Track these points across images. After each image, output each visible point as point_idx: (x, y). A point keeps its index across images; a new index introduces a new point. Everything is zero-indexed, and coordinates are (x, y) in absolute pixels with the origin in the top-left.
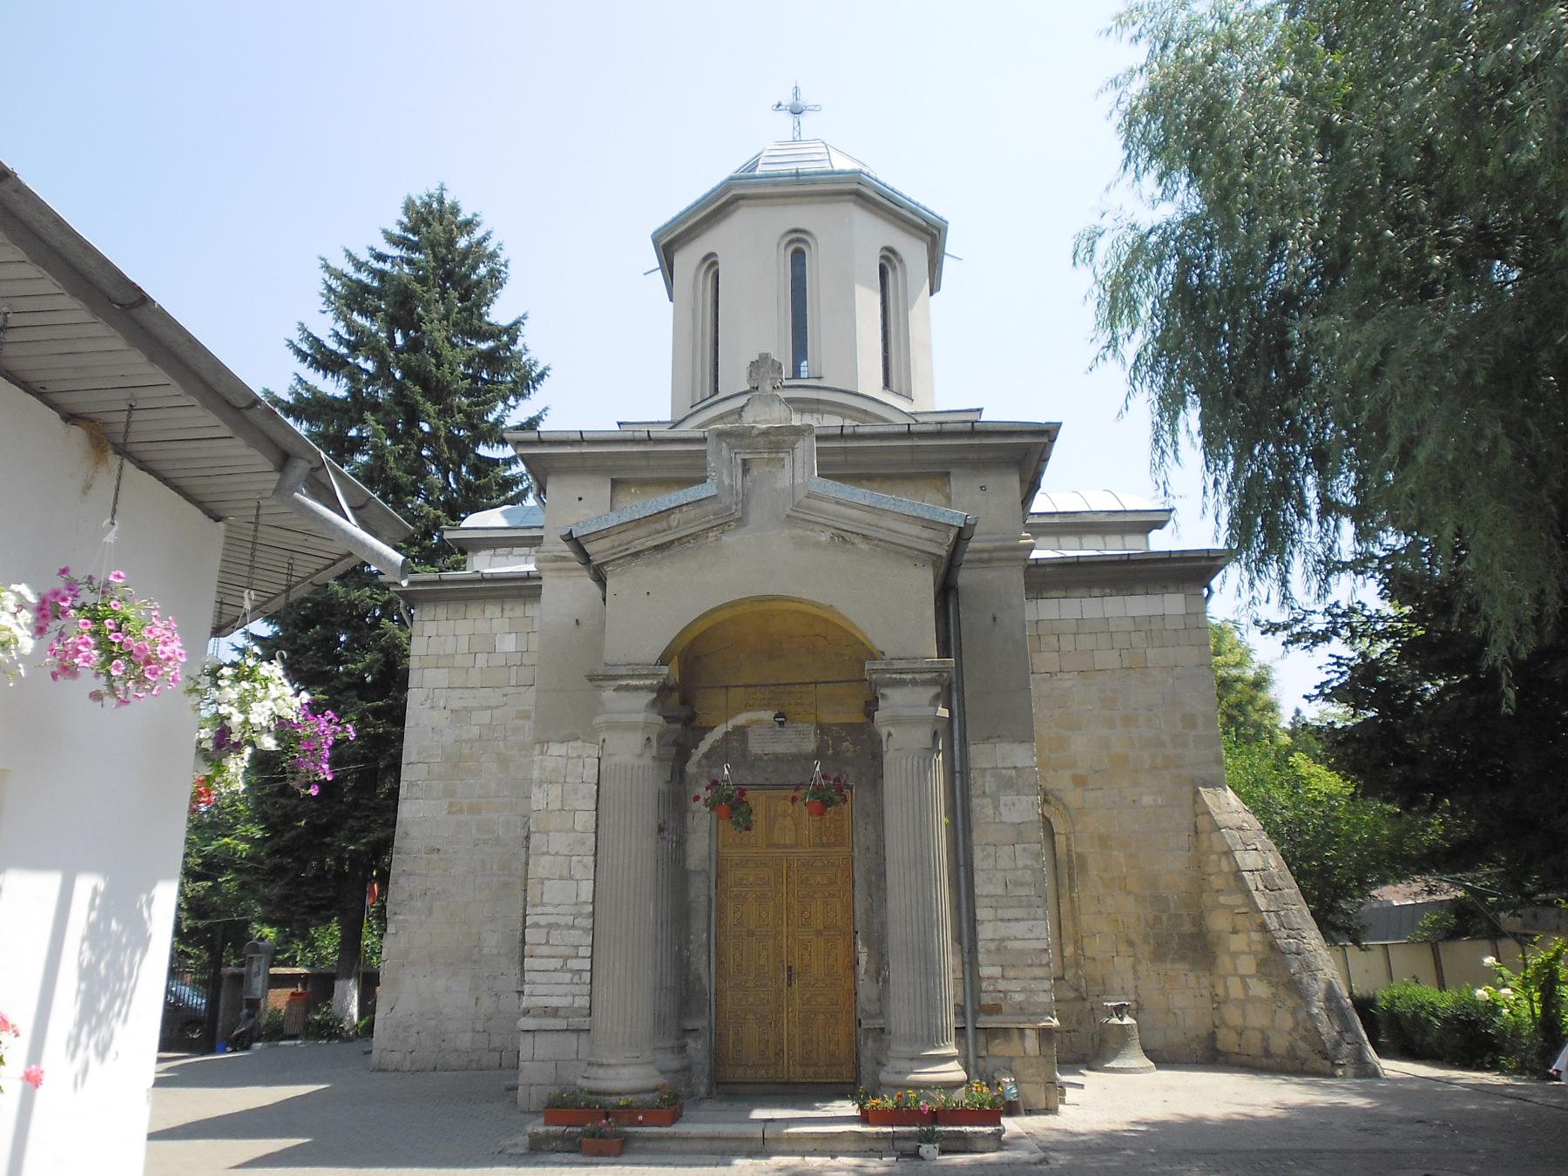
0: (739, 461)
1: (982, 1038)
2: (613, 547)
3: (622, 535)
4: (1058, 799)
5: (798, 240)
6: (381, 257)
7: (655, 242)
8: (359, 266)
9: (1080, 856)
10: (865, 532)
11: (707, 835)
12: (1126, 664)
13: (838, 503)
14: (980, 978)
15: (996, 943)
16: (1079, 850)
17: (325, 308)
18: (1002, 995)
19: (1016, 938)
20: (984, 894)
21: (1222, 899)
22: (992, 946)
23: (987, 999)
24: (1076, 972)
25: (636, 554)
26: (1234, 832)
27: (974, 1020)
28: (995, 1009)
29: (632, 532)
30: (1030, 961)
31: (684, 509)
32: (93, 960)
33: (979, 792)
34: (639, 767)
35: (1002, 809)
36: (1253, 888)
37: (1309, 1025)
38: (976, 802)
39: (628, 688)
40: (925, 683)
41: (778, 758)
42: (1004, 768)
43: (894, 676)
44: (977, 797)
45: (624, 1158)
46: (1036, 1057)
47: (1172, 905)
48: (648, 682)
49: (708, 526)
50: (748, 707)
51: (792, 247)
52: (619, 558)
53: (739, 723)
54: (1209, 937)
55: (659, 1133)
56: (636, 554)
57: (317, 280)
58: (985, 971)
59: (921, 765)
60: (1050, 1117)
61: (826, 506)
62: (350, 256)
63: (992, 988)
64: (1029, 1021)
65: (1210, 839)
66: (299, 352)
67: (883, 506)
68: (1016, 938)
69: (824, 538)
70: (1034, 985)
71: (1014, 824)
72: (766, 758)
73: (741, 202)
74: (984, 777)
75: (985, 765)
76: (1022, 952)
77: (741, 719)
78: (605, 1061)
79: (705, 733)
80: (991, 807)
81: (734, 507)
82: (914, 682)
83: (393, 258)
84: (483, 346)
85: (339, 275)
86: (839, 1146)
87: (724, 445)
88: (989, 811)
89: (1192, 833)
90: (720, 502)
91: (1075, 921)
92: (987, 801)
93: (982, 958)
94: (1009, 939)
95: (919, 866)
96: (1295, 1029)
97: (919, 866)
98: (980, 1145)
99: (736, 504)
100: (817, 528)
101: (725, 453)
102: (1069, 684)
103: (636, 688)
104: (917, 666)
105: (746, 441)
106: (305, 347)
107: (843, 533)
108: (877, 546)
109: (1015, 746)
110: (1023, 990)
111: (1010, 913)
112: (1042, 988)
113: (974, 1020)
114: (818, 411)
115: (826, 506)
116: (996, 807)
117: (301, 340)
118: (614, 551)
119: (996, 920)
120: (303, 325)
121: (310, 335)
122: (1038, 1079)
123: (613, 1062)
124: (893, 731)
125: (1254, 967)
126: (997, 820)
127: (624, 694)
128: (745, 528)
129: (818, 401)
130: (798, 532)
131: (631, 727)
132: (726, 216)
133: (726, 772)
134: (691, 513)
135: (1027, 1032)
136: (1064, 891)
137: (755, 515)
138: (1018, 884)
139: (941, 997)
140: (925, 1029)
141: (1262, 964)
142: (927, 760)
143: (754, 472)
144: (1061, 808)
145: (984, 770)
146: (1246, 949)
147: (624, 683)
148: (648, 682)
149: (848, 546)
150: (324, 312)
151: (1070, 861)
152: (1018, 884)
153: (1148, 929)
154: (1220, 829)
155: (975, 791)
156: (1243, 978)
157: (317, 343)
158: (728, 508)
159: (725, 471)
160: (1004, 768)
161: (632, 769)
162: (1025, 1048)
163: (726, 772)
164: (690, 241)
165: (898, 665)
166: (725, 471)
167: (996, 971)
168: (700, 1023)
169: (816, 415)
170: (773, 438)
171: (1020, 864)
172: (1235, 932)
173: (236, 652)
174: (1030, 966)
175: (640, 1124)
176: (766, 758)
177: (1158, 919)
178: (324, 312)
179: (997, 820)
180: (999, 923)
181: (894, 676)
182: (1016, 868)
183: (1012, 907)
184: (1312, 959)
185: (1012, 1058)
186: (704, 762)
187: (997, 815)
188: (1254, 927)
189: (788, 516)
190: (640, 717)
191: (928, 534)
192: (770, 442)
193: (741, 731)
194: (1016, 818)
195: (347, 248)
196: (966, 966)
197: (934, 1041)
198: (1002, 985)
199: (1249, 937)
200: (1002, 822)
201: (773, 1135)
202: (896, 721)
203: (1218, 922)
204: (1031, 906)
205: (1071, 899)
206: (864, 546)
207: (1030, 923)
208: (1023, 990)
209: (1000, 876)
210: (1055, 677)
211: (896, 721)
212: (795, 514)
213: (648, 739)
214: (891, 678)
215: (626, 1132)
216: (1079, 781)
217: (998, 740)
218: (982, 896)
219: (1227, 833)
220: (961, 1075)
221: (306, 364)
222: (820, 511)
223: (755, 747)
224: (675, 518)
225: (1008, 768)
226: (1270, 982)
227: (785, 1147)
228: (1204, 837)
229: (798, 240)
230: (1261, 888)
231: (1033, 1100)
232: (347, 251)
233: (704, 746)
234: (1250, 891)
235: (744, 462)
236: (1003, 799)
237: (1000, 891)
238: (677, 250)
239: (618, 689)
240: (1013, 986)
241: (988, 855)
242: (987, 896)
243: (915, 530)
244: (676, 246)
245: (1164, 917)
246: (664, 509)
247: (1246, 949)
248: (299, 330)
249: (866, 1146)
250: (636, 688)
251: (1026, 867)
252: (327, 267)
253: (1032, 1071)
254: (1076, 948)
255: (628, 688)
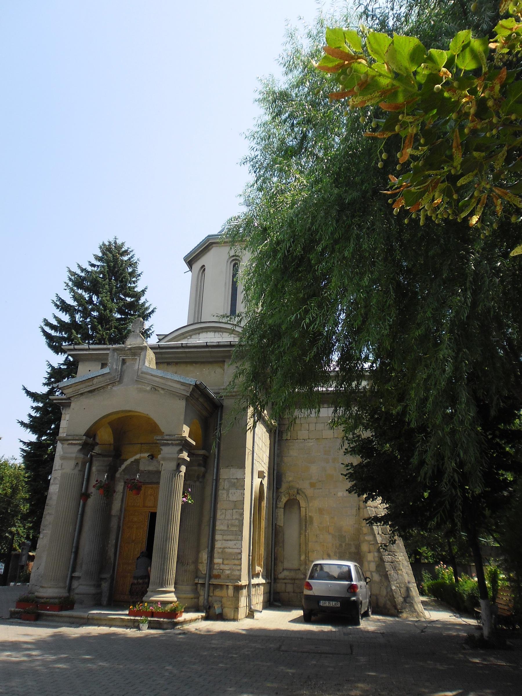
0: (121, 359)
1: (212, 588)
2: (73, 392)
3: (76, 387)
4: (303, 492)
5: (236, 259)
6: (93, 265)
7: (185, 259)
8: (83, 270)
9: (311, 517)
10: (163, 387)
11: (120, 501)
12: (335, 436)
13: (152, 375)
14: (214, 564)
15: (221, 549)
16: (310, 514)
17: (66, 288)
18: (221, 571)
19: (229, 548)
20: (219, 529)
21: (366, 538)
22: (220, 550)
23: (215, 572)
24: (305, 567)
25: (82, 394)
26: (373, 509)
27: (209, 581)
28: (218, 577)
29: (80, 386)
30: (233, 557)
31: (98, 377)
32: (149, 568)
33: (222, 488)
34: (74, 474)
35: (230, 495)
36: (376, 533)
37: (391, 594)
38: (220, 492)
39: (72, 444)
40: (177, 445)
41: (149, 472)
42: (232, 479)
43: (165, 442)
44: (221, 490)
45: (38, 622)
46: (232, 597)
47: (347, 540)
48: (79, 442)
49: (107, 384)
50: (141, 452)
51: (234, 262)
52: (76, 395)
53: (137, 458)
54: (361, 554)
55: (52, 614)
56: (82, 394)
57: (65, 277)
58: (216, 561)
59: (171, 476)
60: (235, 623)
61: (148, 377)
62: (79, 266)
63: (218, 568)
64: (230, 582)
65: (363, 512)
66: (56, 305)
67: (167, 377)
68: (229, 548)
69: (148, 388)
70: (234, 567)
71: (233, 501)
72: (145, 472)
73: (213, 245)
74: (224, 482)
75: (226, 477)
76: (231, 554)
77: (137, 457)
78: (43, 585)
79: (124, 462)
80: (226, 494)
81: (117, 377)
82: (172, 444)
83: (98, 265)
84: (128, 299)
85: (74, 274)
86: (114, 623)
87: (116, 353)
88: (225, 496)
89: (358, 509)
90: (111, 375)
91: (306, 544)
92: (224, 492)
93: (216, 555)
94: (226, 548)
95: (165, 516)
96: (386, 596)
97: (165, 516)
98: (165, 626)
99: (118, 375)
100: (146, 385)
101: (116, 357)
102: (312, 444)
103: (75, 444)
104: (172, 438)
105: (123, 352)
106: (58, 303)
107: (155, 387)
108: (166, 391)
109: (238, 470)
110: (230, 569)
111: (229, 537)
112: (237, 569)
113: (209, 581)
114: (221, 332)
115: (148, 377)
116: (228, 494)
117: (57, 301)
118: (73, 393)
119: (223, 540)
120: (57, 294)
121: (60, 298)
122: (231, 606)
123: (46, 586)
124: (163, 463)
125: (375, 568)
126: (227, 499)
127: (70, 446)
128: (122, 384)
129: (221, 328)
130: (140, 386)
131: (70, 458)
132: (209, 250)
133: (138, 477)
134: (101, 379)
135: (230, 587)
136: (303, 532)
137: (126, 379)
138: (233, 525)
139: (167, 568)
140: (158, 580)
141: (378, 566)
142: (174, 475)
143: (127, 364)
144: (304, 496)
145: (225, 479)
146: (373, 560)
147: (70, 442)
148: (79, 442)
149: (157, 392)
150: (66, 289)
151: (306, 519)
152: (233, 525)
153: (336, 550)
154: (367, 507)
155: (221, 487)
156: (371, 572)
157: (63, 302)
158: (114, 377)
159: (115, 363)
160: (232, 479)
161: (69, 474)
162: (228, 593)
163: (138, 477)
164: (197, 261)
165: (167, 437)
166: (115, 363)
167: (220, 561)
168: (107, 576)
169: (220, 333)
170: (133, 351)
171: (234, 517)
172: (370, 552)
173: (19, 424)
174: (234, 559)
175: (48, 610)
176: (145, 472)
177: (341, 545)
178: (66, 289)
179: (227, 499)
180: (224, 541)
181: (165, 442)
182: (233, 519)
183: (229, 535)
184: (397, 565)
185: (222, 597)
186: (123, 473)
187: (228, 498)
188: (376, 550)
189: (136, 380)
190: (74, 455)
191: (182, 387)
192: (132, 352)
193: (137, 461)
194: (235, 499)
195: (78, 263)
196: (209, 558)
197: (162, 585)
198: (222, 567)
199: (374, 554)
200: (229, 501)
201: (91, 617)
202: (164, 459)
203: (365, 548)
204: (236, 535)
205: (305, 535)
206: (162, 392)
207: (235, 542)
208: (230, 569)
209: (226, 522)
210: (306, 441)
211: (164, 459)
212: (138, 380)
213: (77, 463)
214: (164, 442)
215: (39, 612)
216: (312, 485)
217: (231, 467)
218: (218, 530)
219: (369, 509)
220: (175, 599)
221: (59, 310)
222: (146, 378)
223: (142, 468)
224: (95, 381)
225: (234, 479)
226: (380, 575)
227: (104, 623)
228: (361, 510)
229: (236, 259)
230: (380, 533)
231: (229, 615)
232: (78, 264)
233: (123, 467)
234: (375, 534)
235: (123, 360)
236: (230, 491)
237: (226, 528)
238: (193, 264)
239: (69, 444)
240: (227, 567)
241: (223, 514)
242: (220, 530)
243: (178, 386)
244: (193, 262)
245: (344, 545)
246: (90, 377)
247: (373, 560)
248: (56, 296)
249: (124, 624)
250: (75, 444)
251: (236, 519)
252: (70, 271)
253: (229, 603)
254: (306, 556)
255: (72, 444)
